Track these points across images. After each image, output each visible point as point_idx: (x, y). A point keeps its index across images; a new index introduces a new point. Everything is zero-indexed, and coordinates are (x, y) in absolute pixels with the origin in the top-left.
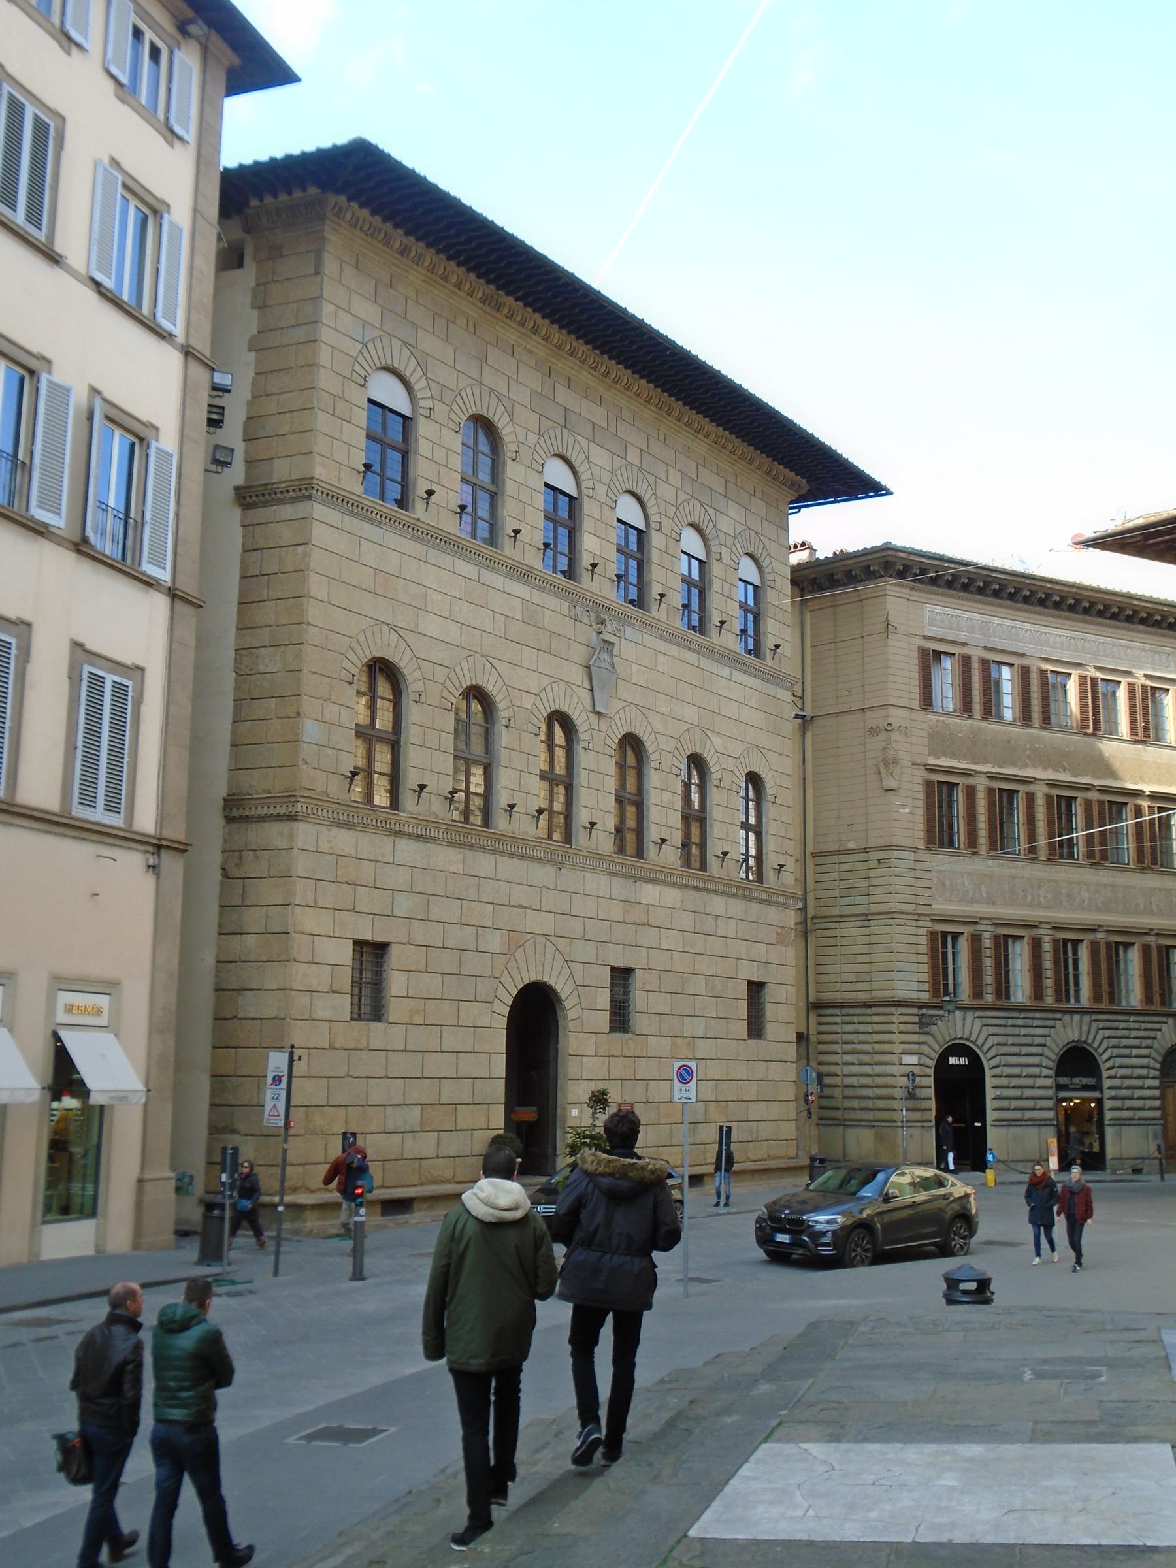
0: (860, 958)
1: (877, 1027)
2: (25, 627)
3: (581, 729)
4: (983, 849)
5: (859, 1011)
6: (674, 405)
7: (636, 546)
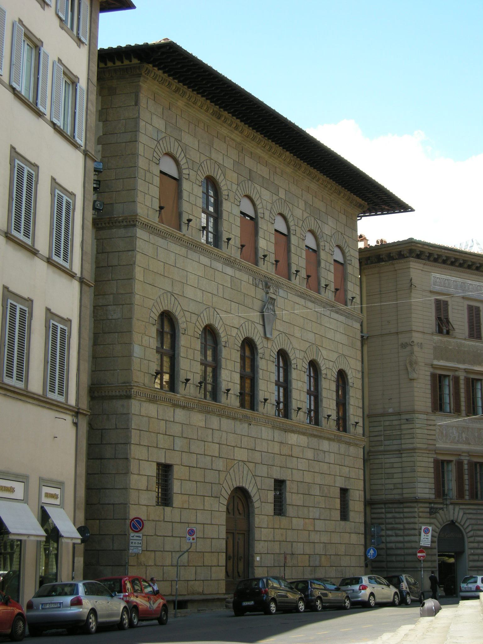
2: (30, 302)
3: (259, 347)
4: (463, 413)
5: (395, 506)
6: (302, 165)
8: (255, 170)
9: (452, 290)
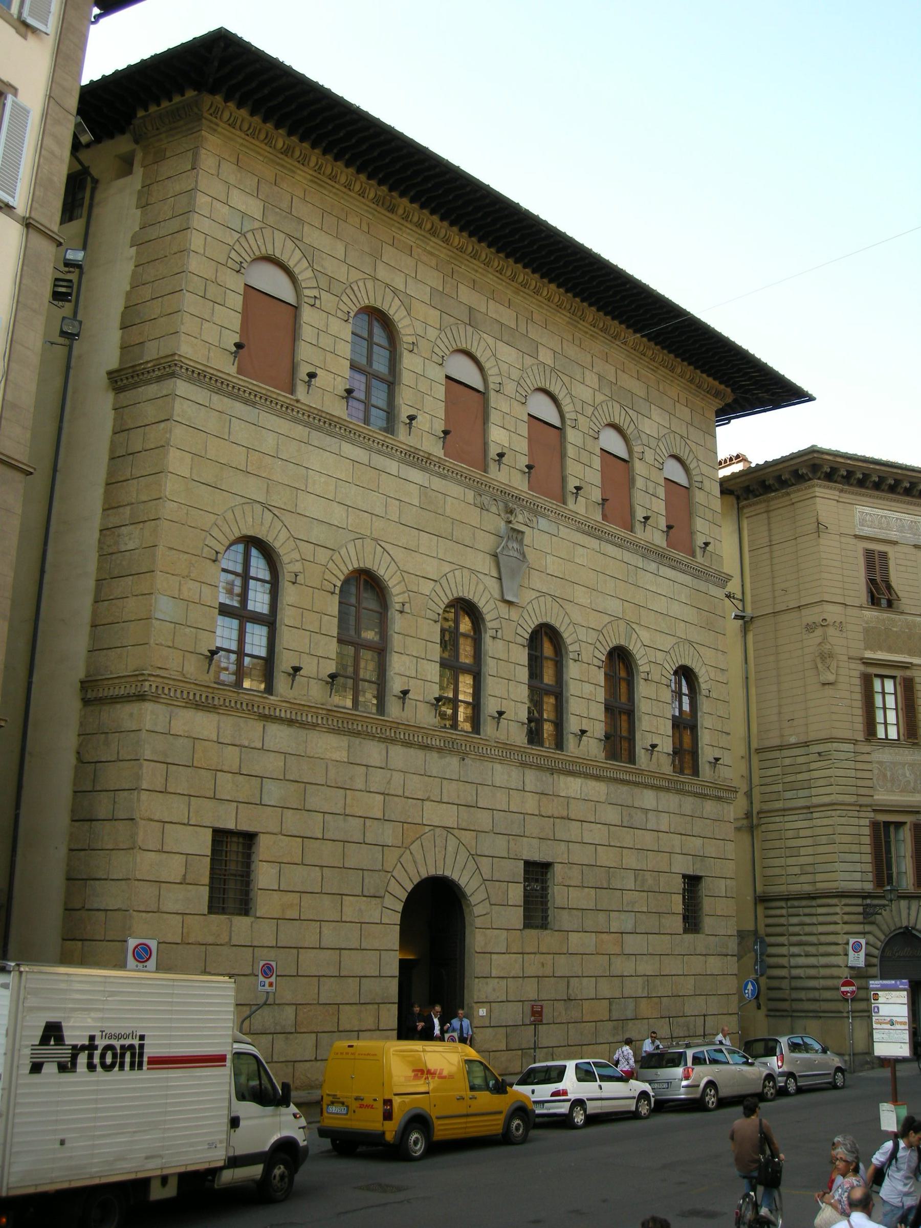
0: (803, 851)
1: (821, 919)
3: (488, 617)
5: (804, 903)
7: (548, 437)
8: (484, 310)
9: (893, 535)
